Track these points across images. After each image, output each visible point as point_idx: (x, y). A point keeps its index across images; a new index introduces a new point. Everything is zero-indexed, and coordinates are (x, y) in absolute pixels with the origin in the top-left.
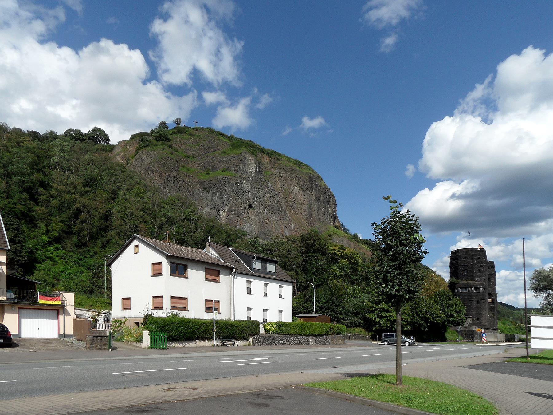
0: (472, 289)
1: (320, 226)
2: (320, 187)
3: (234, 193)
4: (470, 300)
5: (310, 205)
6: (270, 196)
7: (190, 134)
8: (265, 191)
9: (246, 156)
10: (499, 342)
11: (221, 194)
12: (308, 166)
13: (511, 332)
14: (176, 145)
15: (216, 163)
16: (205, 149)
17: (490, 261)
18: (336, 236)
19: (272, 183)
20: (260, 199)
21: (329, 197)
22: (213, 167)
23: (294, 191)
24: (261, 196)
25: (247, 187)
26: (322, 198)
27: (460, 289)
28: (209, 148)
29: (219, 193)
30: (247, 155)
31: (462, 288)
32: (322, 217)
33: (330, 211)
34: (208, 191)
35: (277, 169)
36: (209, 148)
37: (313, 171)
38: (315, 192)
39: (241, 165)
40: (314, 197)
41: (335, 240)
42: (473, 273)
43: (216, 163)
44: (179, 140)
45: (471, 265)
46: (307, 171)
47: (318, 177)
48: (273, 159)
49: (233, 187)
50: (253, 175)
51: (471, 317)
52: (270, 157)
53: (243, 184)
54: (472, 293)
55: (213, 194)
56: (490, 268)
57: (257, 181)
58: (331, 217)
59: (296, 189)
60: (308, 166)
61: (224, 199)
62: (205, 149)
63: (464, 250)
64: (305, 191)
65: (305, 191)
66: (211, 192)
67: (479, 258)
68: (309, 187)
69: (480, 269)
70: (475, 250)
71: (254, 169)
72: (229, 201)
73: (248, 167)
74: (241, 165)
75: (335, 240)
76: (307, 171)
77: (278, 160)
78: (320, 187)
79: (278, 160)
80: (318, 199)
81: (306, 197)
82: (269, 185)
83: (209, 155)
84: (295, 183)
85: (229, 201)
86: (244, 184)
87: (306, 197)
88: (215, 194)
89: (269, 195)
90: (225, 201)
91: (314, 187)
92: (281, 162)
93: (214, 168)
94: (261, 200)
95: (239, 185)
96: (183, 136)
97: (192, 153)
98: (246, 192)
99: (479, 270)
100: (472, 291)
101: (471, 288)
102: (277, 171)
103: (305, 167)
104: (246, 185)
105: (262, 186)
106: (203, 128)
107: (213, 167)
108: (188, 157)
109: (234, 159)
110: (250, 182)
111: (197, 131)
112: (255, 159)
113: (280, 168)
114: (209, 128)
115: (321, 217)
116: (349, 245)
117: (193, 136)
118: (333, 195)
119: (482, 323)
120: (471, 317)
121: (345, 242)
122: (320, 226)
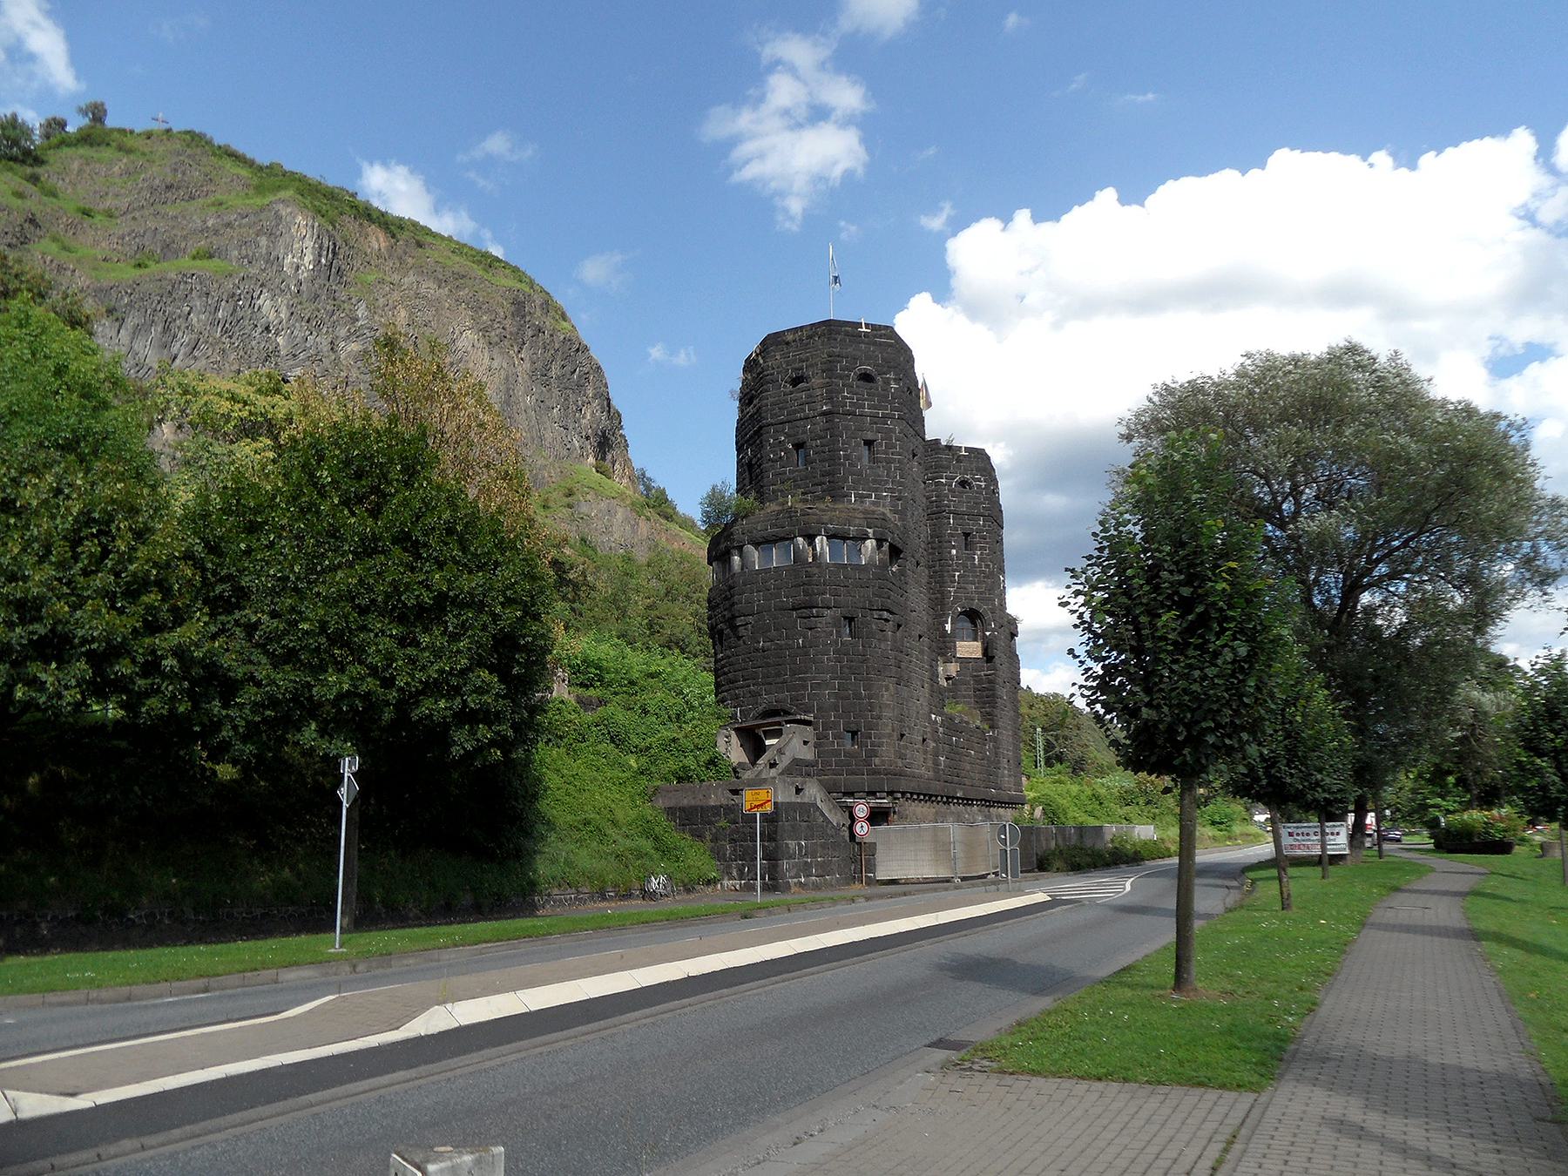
0: (814, 549)
1: (539, 462)
2: (552, 335)
3: (219, 329)
4: (806, 612)
5: (508, 389)
6: (361, 348)
7: (120, 148)
8: (343, 332)
9: (284, 211)
10: (963, 879)
11: (166, 330)
12: (515, 270)
13: (1098, 814)
14: (63, 180)
15: (179, 234)
16: (153, 190)
17: (867, 325)
18: (589, 497)
19: (373, 310)
20: (317, 359)
21: (580, 371)
22: (166, 246)
23: (459, 344)
24: (325, 347)
25: (272, 316)
26: (555, 371)
27: (754, 554)
28: (169, 187)
29: (160, 329)
30: (289, 210)
31: (763, 542)
32: (552, 432)
33: (583, 418)
34: (121, 321)
35: (411, 272)
36: (169, 187)
37: (532, 284)
38: (532, 351)
39: (263, 241)
40: (527, 365)
41: (584, 509)
42: (833, 459)
43: (179, 234)
44: (75, 166)
45: (824, 414)
46: (512, 283)
47: (548, 305)
48: (401, 242)
49: (217, 309)
50: (303, 275)
51: (808, 723)
52: (393, 236)
53: (260, 302)
54: (816, 570)
55: (136, 331)
56: (969, 484)
57: (317, 296)
58: (588, 438)
59: (468, 339)
60: (518, 270)
61: (174, 350)
62: (153, 190)
63: (790, 337)
64: (497, 344)
65: (497, 344)
66: (130, 322)
67: (866, 377)
68: (511, 333)
69: (870, 436)
70: (847, 334)
71: (308, 258)
72: (195, 358)
73: (289, 248)
74: (263, 241)
75: (584, 509)
76: (512, 283)
77: (420, 245)
78: (552, 335)
79: (420, 245)
80: (541, 375)
81: (495, 364)
82: (361, 312)
83: (159, 207)
84: (466, 319)
85: (195, 358)
86: (264, 302)
87: (495, 364)
88: (142, 332)
89: (354, 347)
90: (180, 357)
91: (530, 333)
92: (428, 252)
93: (169, 249)
94: (321, 360)
95: (241, 303)
96: (95, 155)
97: (109, 202)
98: (267, 329)
99: (869, 443)
100: (814, 556)
101: (810, 539)
102: (410, 279)
103: (507, 271)
104: (269, 307)
105: (333, 314)
106: (168, 131)
107: (166, 246)
108: (87, 213)
109: (244, 221)
110: (288, 296)
111: (148, 141)
112: (317, 224)
113: (420, 270)
114: (189, 132)
115: (548, 436)
116: (633, 526)
117: (129, 151)
118: (599, 368)
119: (877, 761)
120: (808, 723)
121: (619, 515)
122: (539, 462)
